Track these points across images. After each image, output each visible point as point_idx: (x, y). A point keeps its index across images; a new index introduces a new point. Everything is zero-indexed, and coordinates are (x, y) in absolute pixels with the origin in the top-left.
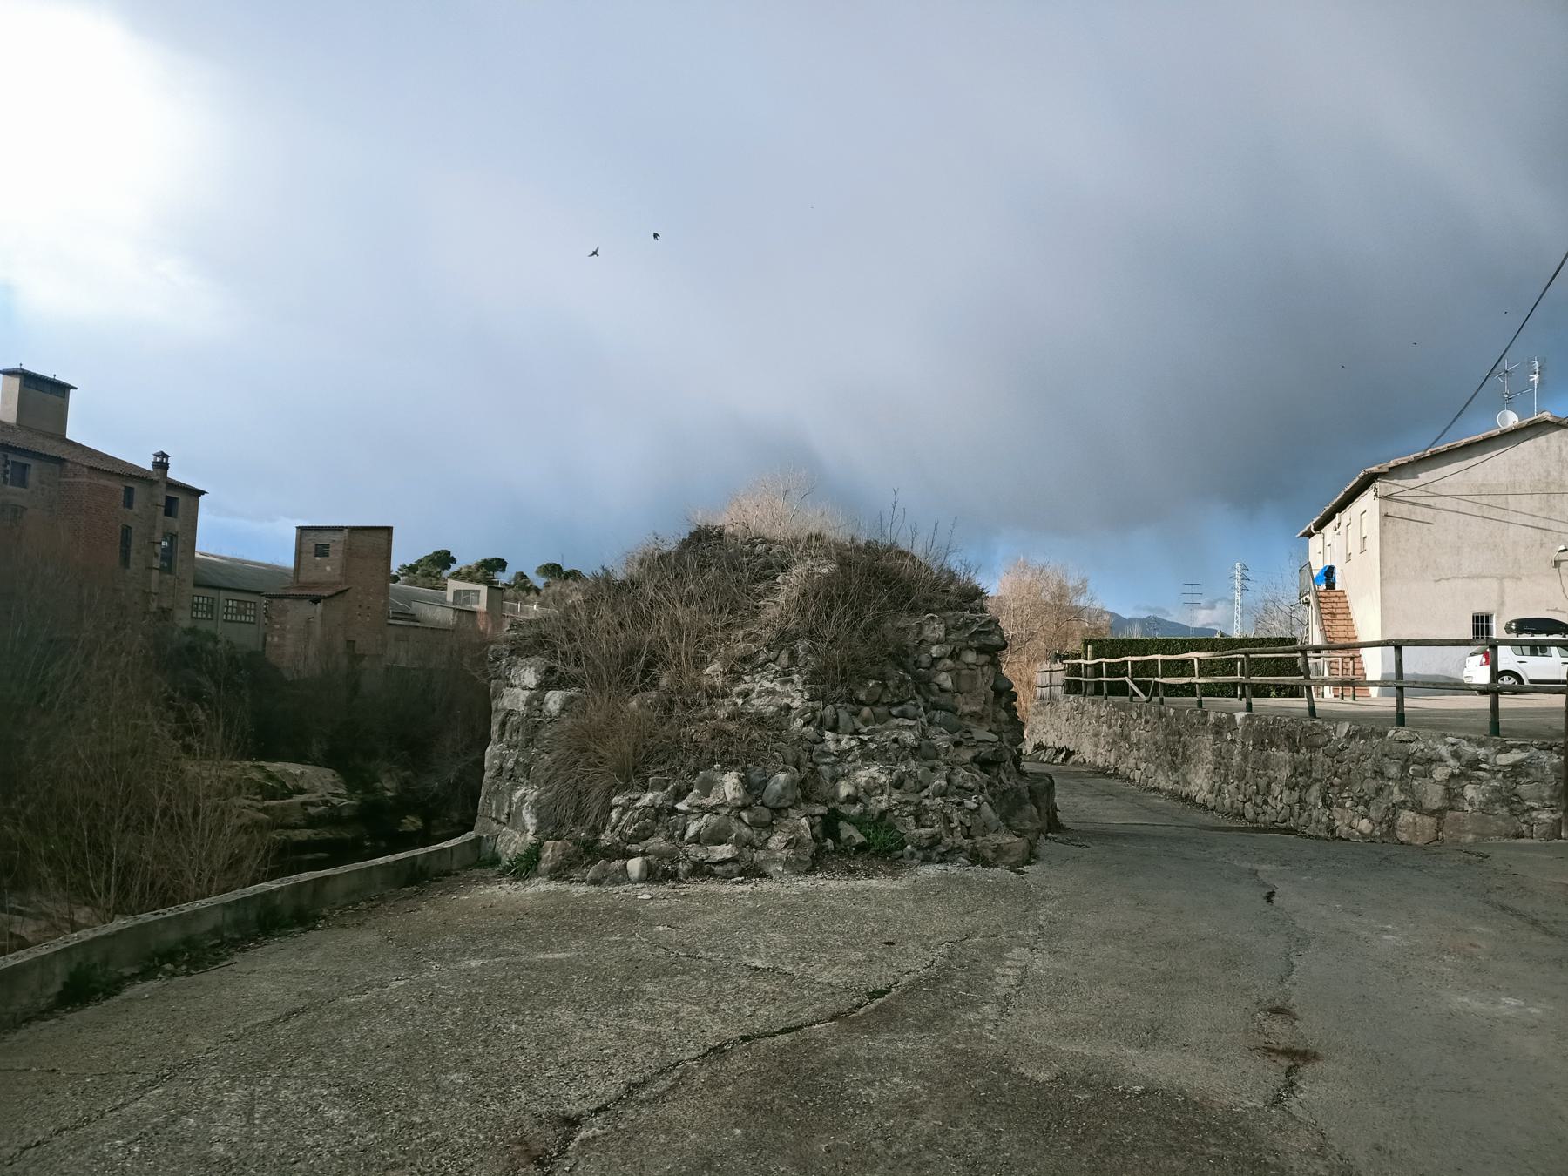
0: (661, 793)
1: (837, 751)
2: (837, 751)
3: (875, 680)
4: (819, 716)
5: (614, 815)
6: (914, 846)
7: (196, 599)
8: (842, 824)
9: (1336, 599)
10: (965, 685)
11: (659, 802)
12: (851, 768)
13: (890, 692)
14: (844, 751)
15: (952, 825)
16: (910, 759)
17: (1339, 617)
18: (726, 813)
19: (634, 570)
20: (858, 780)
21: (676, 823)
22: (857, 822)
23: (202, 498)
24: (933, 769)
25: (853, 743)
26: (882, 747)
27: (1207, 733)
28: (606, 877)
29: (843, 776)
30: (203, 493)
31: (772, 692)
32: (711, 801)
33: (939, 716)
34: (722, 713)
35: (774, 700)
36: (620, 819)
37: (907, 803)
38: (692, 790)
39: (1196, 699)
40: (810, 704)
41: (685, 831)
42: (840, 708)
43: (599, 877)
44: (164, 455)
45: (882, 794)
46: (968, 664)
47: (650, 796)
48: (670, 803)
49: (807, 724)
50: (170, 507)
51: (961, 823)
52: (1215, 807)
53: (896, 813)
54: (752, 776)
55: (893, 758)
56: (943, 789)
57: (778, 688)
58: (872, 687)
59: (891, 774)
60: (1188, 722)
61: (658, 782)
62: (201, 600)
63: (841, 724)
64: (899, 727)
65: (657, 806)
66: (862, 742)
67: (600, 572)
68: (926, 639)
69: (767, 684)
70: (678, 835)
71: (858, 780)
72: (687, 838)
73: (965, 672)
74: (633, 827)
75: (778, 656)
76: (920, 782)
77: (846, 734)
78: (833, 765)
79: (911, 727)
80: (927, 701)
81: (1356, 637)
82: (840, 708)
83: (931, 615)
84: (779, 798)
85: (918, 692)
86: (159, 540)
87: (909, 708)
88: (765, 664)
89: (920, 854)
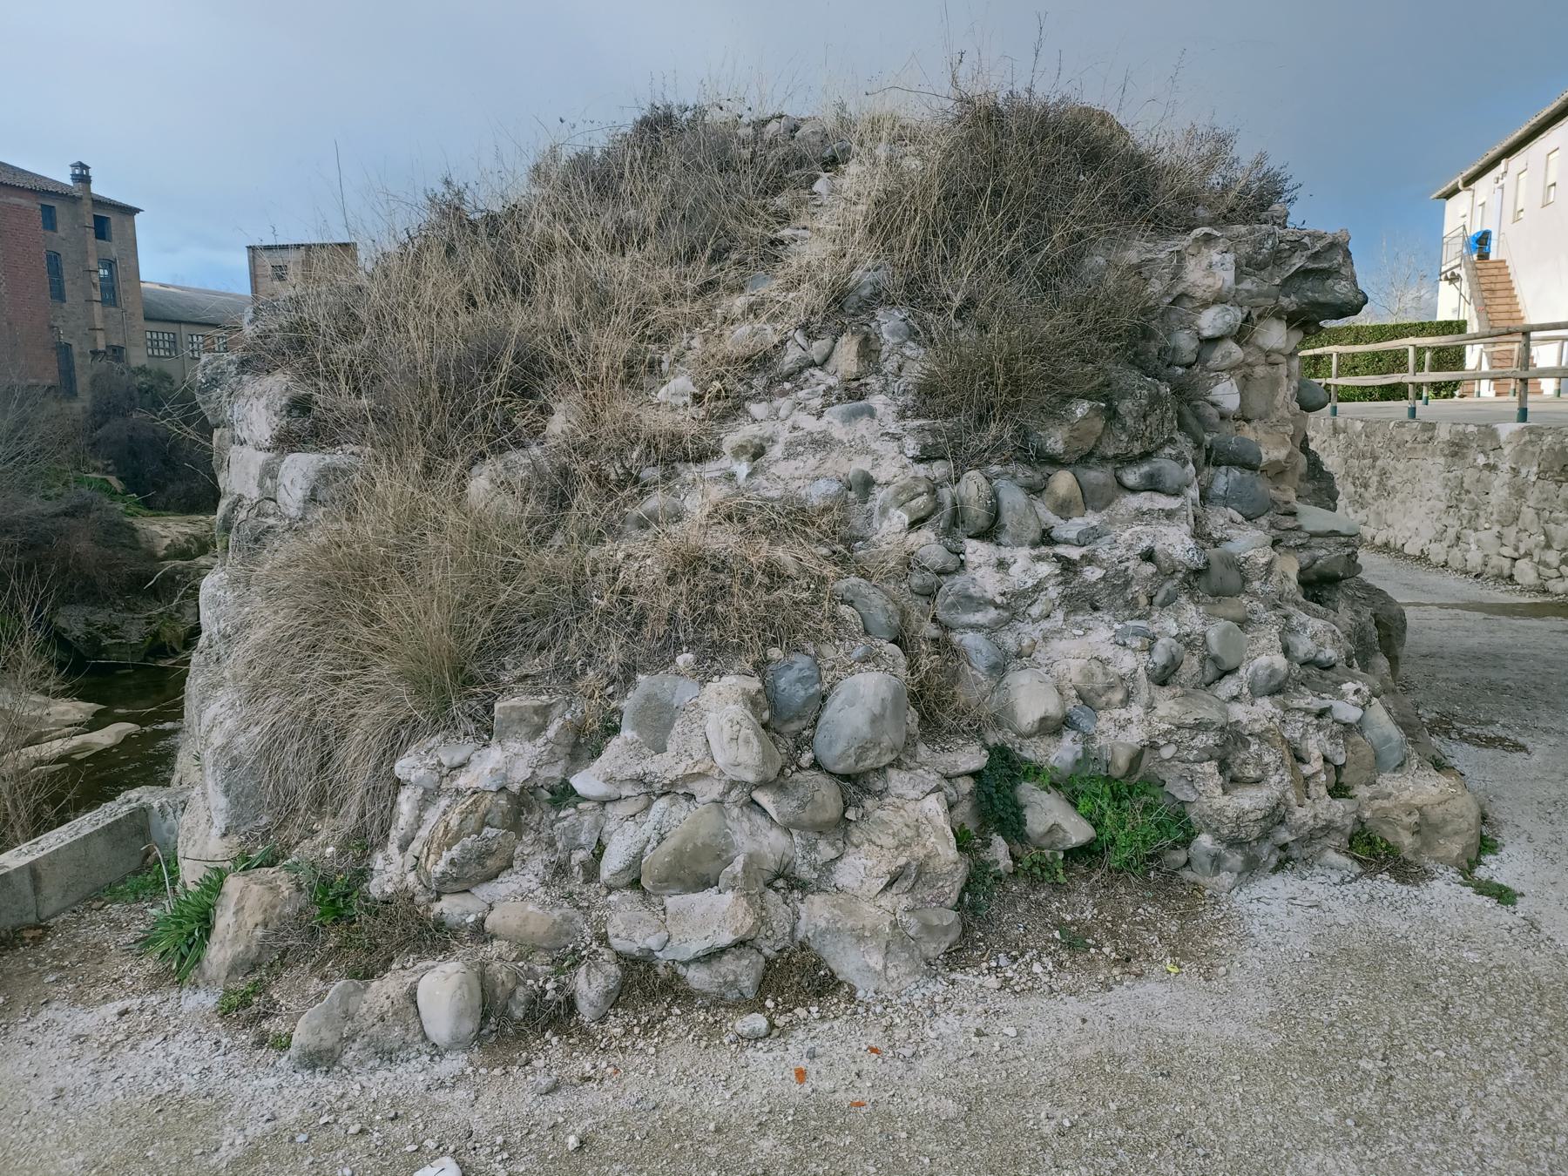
0: (528, 746)
1: (1003, 594)
2: (1003, 594)
3: (1090, 400)
4: (948, 501)
5: (406, 804)
6: (1220, 839)
7: (148, 334)
8: (1028, 792)
9: (1495, 272)
10: (1257, 403)
11: (520, 774)
12: (1037, 635)
13: (1124, 427)
14: (1021, 595)
15: (1307, 770)
16: (1183, 599)
17: (1499, 294)
18: (715, 796)
19: (520, 188)
20: (1059, 668)
21: (575, 830)
22: (1069, 787)
23: (137, 217)
24: (1243, 623)
25: (1044, 569)
26: (1117, 574)
27: (1433, 455)
28: (351, 1038)
29: (1019, 655)
30: (137, 211)
31: (822, 443)
32: (665, 766)
33: (1224, 479)
34: (696, 505)
35: (829, 464)
36: (419, 821)
37: (1200, 726)
38: (616, 730)
39: (1405, 404)
40: (921, 470)
41: (600, 849)
42: (998, 476)
43: (327, 1044)
44: (82, 166)
45: (1127, 701)
46: (1268, 354)
47: (494, 756)
48: (556, 772)
49: (916, 524)
50: (101, 229)
51: (1326, 760)
52: (1446, 563)
53: (1167, 753)
54: (782, 683)
55: (1143, 600)
56: (1280, 678)
57: (838, 431)
58: (1084, 418)
59: (1150, 650)
60: (1391, 439)
61: (515, 715)
62: (155, 336)
63: (1008, 518)
64: (1140, 514)
65: (515, 788)
66: (1068, 566)
67: (440, 189)
68: (1191, 291)
69: (809, 424)
70: (582, 864)
71: (1059, 668)
72: (605, 874)
73: (1260, 371)
74: (446, 855)
75: (832, 349)
76: (1215, 660)
77: (1022, 545)
78: (991, 630)
79: (1170, 515)
80: (1198, 445)
81: (1522, 319)
82: (998, 476)
83: (1207, 230)
84: (862, 751)
85: (1182, 426)
86: (96, 267)
87: (1164, 464)
88: (801, 370)
89: (1236, 859)
